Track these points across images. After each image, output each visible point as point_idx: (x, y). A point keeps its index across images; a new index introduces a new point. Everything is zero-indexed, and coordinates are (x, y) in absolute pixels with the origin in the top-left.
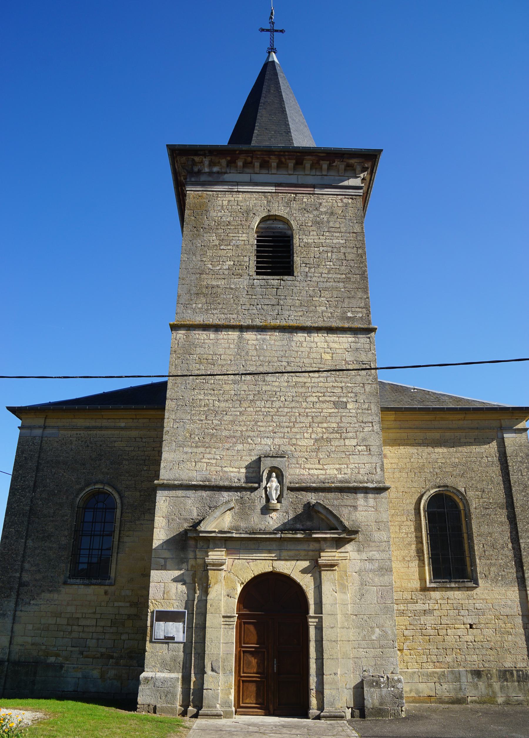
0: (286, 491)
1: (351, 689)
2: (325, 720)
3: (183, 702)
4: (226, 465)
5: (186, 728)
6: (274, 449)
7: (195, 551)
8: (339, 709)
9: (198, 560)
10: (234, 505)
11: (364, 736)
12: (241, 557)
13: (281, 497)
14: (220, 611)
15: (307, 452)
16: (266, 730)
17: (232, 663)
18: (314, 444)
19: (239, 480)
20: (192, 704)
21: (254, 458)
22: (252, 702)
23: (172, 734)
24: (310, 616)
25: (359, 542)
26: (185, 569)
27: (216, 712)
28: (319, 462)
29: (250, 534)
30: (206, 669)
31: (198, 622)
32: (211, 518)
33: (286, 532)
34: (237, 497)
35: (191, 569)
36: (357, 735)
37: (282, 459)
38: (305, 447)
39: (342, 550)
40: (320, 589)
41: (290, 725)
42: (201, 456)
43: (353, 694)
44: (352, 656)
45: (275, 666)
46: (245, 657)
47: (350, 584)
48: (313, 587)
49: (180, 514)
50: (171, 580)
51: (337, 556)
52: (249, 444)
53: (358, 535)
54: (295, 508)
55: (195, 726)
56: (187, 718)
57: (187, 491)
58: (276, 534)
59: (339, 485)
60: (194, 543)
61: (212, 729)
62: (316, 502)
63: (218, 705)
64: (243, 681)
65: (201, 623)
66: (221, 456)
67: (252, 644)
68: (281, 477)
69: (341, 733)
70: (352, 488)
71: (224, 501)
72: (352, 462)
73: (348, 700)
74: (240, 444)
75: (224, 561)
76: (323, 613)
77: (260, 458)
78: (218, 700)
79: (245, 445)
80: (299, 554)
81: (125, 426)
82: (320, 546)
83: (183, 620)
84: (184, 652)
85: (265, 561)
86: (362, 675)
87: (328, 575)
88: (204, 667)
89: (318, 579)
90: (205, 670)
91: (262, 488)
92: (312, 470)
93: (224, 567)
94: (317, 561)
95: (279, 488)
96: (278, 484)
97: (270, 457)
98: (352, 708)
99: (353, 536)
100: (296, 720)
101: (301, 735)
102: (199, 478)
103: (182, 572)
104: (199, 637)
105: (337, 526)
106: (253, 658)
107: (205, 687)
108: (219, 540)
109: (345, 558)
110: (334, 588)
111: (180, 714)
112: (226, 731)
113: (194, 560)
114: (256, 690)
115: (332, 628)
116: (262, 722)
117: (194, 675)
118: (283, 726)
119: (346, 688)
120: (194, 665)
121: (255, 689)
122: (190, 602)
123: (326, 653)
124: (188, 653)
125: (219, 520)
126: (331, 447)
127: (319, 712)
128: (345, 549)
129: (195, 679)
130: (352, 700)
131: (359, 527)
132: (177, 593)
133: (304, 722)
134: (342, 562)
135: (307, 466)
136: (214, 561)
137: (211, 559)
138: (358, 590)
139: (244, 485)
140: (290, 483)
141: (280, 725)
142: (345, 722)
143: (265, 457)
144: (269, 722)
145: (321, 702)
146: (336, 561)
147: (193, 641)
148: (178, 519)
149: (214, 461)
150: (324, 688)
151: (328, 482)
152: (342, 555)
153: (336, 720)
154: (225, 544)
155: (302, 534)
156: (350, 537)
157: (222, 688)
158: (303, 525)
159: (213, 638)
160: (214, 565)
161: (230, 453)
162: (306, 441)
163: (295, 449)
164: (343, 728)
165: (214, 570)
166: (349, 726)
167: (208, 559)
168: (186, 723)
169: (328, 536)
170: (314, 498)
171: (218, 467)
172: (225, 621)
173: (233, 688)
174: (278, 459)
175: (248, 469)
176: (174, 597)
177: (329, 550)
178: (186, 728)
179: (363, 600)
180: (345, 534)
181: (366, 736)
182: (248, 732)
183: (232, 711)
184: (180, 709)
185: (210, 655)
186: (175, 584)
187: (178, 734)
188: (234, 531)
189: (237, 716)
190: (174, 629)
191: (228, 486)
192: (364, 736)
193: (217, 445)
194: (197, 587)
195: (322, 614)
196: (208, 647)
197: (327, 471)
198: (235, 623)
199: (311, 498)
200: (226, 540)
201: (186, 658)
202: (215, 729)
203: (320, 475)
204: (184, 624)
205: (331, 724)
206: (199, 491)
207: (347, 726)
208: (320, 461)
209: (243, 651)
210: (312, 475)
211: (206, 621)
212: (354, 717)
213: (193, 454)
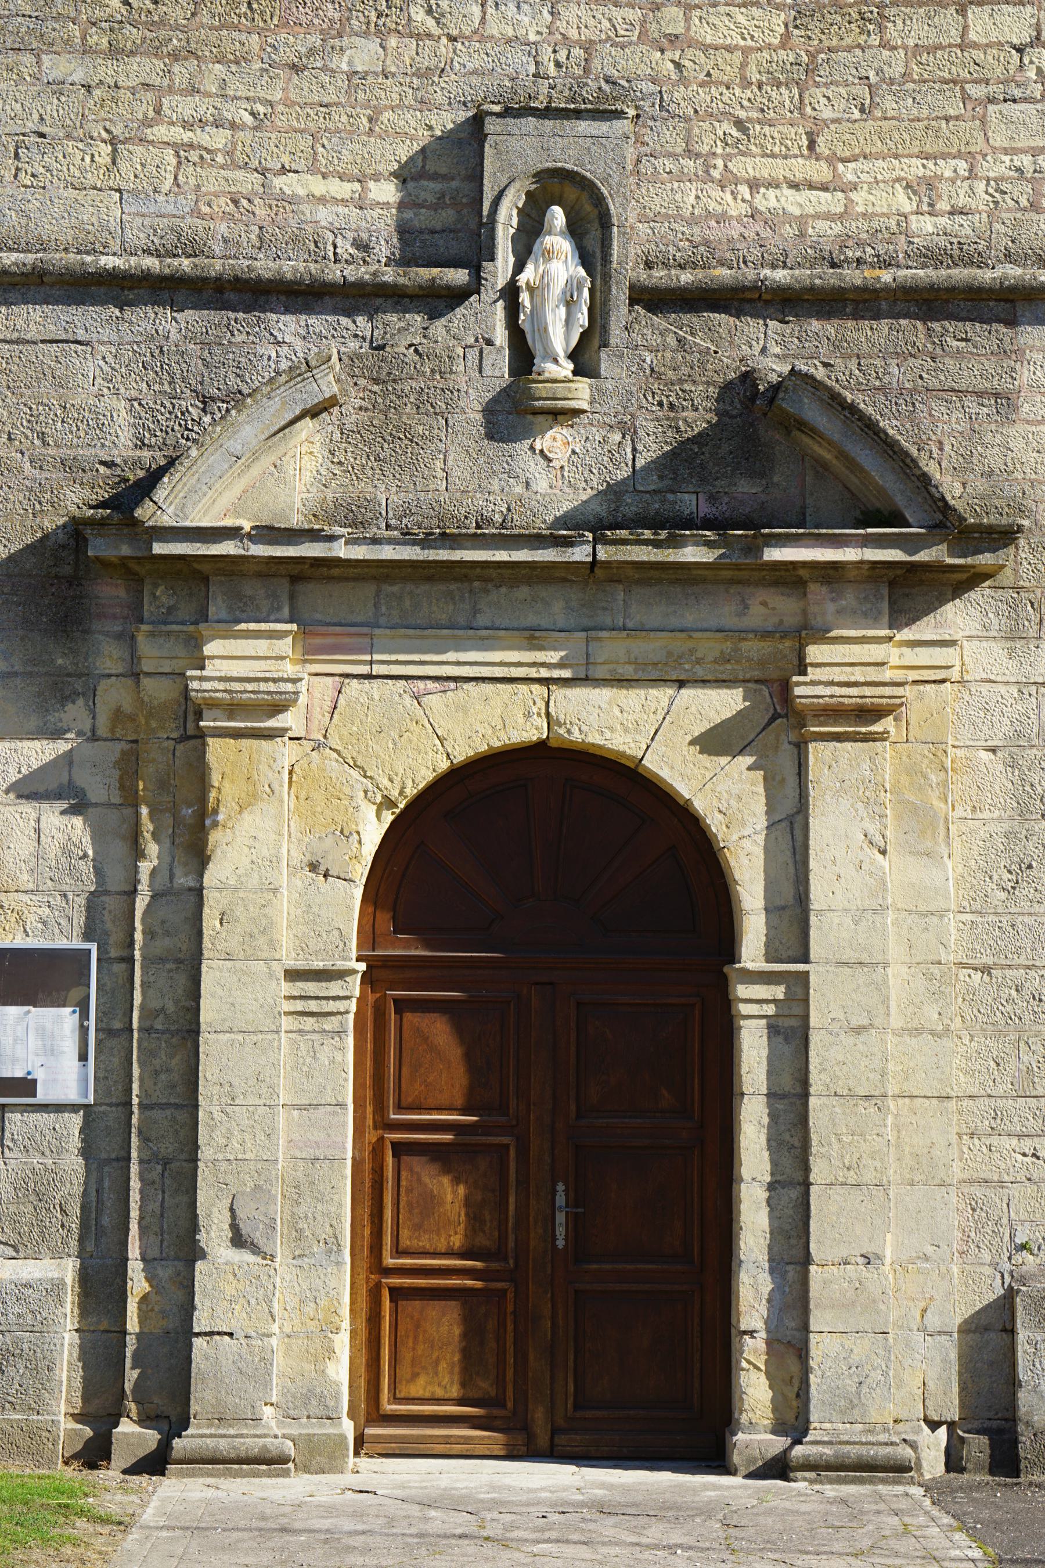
0: (624, 309)
1: (950, 1334)
2: (812, 1482)
3: (85, 1398)
4: (286, 159)
5: (104, 1521)
6: (558, 65)
7: (133, 638)
8: (886, 1430)
9: (145, 681)
10: (335, 389)
11: (1013, 1561)
12: (377, 669)
13: (596, 342)
14: (273, 945)
15: (746, 84)
16: (513, 1527)
17: (340, 1205)
18: (787, 36)
19: (363, 246)
20: (133, 1406)
21: (447, 120)
22: (440, 1393)
23: (37, 1555)
24: (745, 972)
25: (1018, 589)
26: (80, 734)
27: (261, 1441)
28: (812, 145)
29: (425, 543)
30: (202, 1237)
31: (155, 1004)
32: (214, 459)
33: (624, 533)
34: (353, 345)
35: (112, 731)
36: (977, 1554)
37: (601, 128)
38: (737, 57)
39: (924, 629)
40: (798, 832)
41: (636, 1505)
42: (144, 109)
43: (960, 1357)
44: (957, 1171)
45: (560, 1218)
46: (404, 1174)
47: (959, 812)
48: (762, 823)
49: (42, 436)
50: (7, 792)
51: (894, 661)
52: (418, 37)
53: (1011, 550)
54: (672, 406)
55: (150, 1511)
56: (110, 1475)
57: (73, 309)
58: (566, 543)
59: (922, 274)
60: (122, 593)
61: (242, 1524)
62: (786, 369)
63: (268, 1412)
64: (396, 1293)
65: (171, 1007)
66: (261, 109)
67: (439, 1109)
68: (594, 233)
69: (894, 1544)
70: (991, 290)
71: (284, 365)
72: (998, 140)
73: (931, 1384)
74: (366, 34)
75: (289, 687)
76: (813, 955)
77: (478, 120)
78: (266, 1385)
79: (393, 42)
80: (692, 651)
81: (123, 289)
82: (804, 612)
83: (75, 994)
84: (86, 1152)
85: (509, 687)
86: (1007, 1267)
87: (843, 762)
88: (193, 1226)
89: (792, 781)
90: (196, 1242)
91: (489, 294)
92: (771, 193)
93: (290, 720)
94: (785, 688)
95: (586, 293)
96: (582, 272)
97: (534, 112)
98: (951, 1425)
99: (985, 559)
100: (664, 1478)
101: (690, 1548)
102: (136, 236)
103: (62, 747)
104: (163, 1076)
105: (900, 501)
106: (446, 1180)
107: (201, 1321)
108: (259, 575)
109: (940, 675)
110: (872, 829)
111: (75, 1456)
112: (311, 1531)
113: (130, 682)
114: (465, 1335)
115: (859, 1030)
116: (493, 1488)
117: (140, 1265)
118: (603, 1509)
119: (923, 1329)
120: (141, 1218)
121: (457, 1331)
122: (112, 903)
123: (823, 1156)
124: (108, 1161)
125: (255, 471)
126: (886, 53)
127: (780, 1443)
128: (939, 625)
129: (146, 1287)
130: (956, 1389)
131: (1021, 511)
132: (39, 855)
133: (706, 1487)
134: (921, 696)
135: (745, 167)
136: (237, 686)
137: (220, 679)
138: (999, 840)
139: (389, 275)
140: (649, 265)
141: (583, 1504)
142: (917, 1491)
143: (507, 112)
144: (530, 1491)
145: (792, 1395)
146: (887, 691)
147: (135, 1101)
148: (27, 466)
149: (219, 138)
150: (812, 1328)
151: (859, 261)
152: (913, 657)
153: (871, 1481)
154: (292, 597)
155: (709, 544)
156: (969, 560)
157: (287, 1329)
158: (712, 498)
159: (236, 1081)
160: (233, 709)
161: (304, 88)
162: (741, 19)
163: (678, 65)
164: (907, 1520)
165: (237, 734)
166: (935, 1512)
167: (201, 679)
168: (108, 1496)
169: (849, 554)
170: (777, 350)
171: (240, 174)
172: (302, 997)
173: (346, 1325)
174: (583, 126)
175: (411, 185)
176: (25, 880)
177: (852, 633)
178: (104, 1521)
179: (1025, 891)
180: (944, 547)
181: (1026, 1561)
182: (420, 1535)
183: (343, 1437)
184: (71, 1434)
185: (223, 1166)
186: (28, 808)
187: (67, 1550)
188: (339, 530)
189: (364, 1462)
190: (33, 1042)
191: (299, 283)
192: (1013, 1561)
193: (231, 41)
194: (147, 826)
195: (806, 960)
196: (212, 1129)
197: (853, 195)
198: (353, 1008)
199: (764, 351)
200: (295, 579)
201: (100, 1181)
202: (255, 1524)
203: (817, 216)
204: (84, 1015)
205: (843, 1501)
206: (140, 311)
207: (926, 1513)
208: (820, 140)
209: (396, 1146)
210: (772, 220)
211: (196, 995)
212: (961, 1470)
213: (97, 93)
